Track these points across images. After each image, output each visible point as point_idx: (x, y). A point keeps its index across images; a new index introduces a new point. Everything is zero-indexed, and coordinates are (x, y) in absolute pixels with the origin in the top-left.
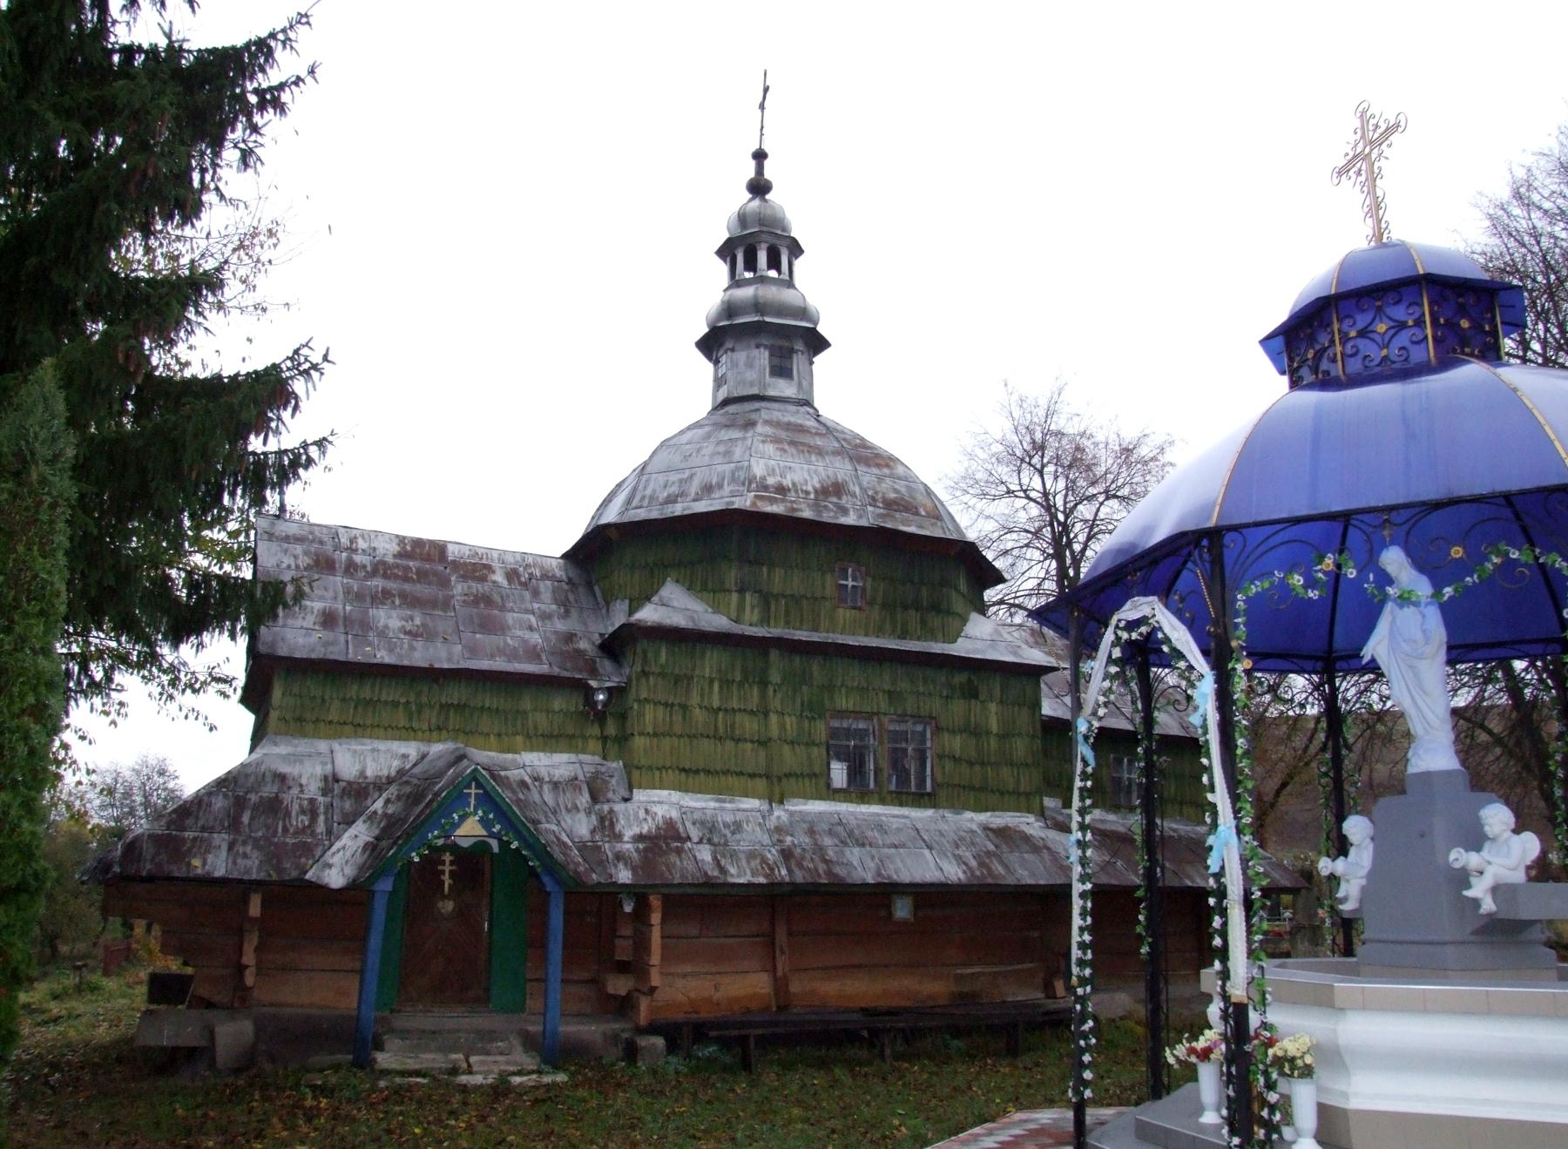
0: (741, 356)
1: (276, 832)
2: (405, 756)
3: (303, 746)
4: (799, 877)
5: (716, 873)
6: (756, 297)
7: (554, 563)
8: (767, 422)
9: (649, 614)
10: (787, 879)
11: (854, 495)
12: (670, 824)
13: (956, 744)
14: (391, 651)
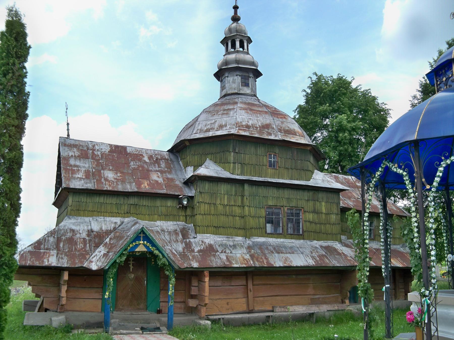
0: (230, 79)
1: (72, 249)
2: (116, 223)
3: (80, 219)
4: (257, 264)
5: (228, 263)
6: (236, 58)
7: (165, 153)
8: (241, 103)
9: (202, 171)
10: (253, 265)
11: (273, 128)
12: (211, 246)
13: (310, 216)
14: (110, 185)
